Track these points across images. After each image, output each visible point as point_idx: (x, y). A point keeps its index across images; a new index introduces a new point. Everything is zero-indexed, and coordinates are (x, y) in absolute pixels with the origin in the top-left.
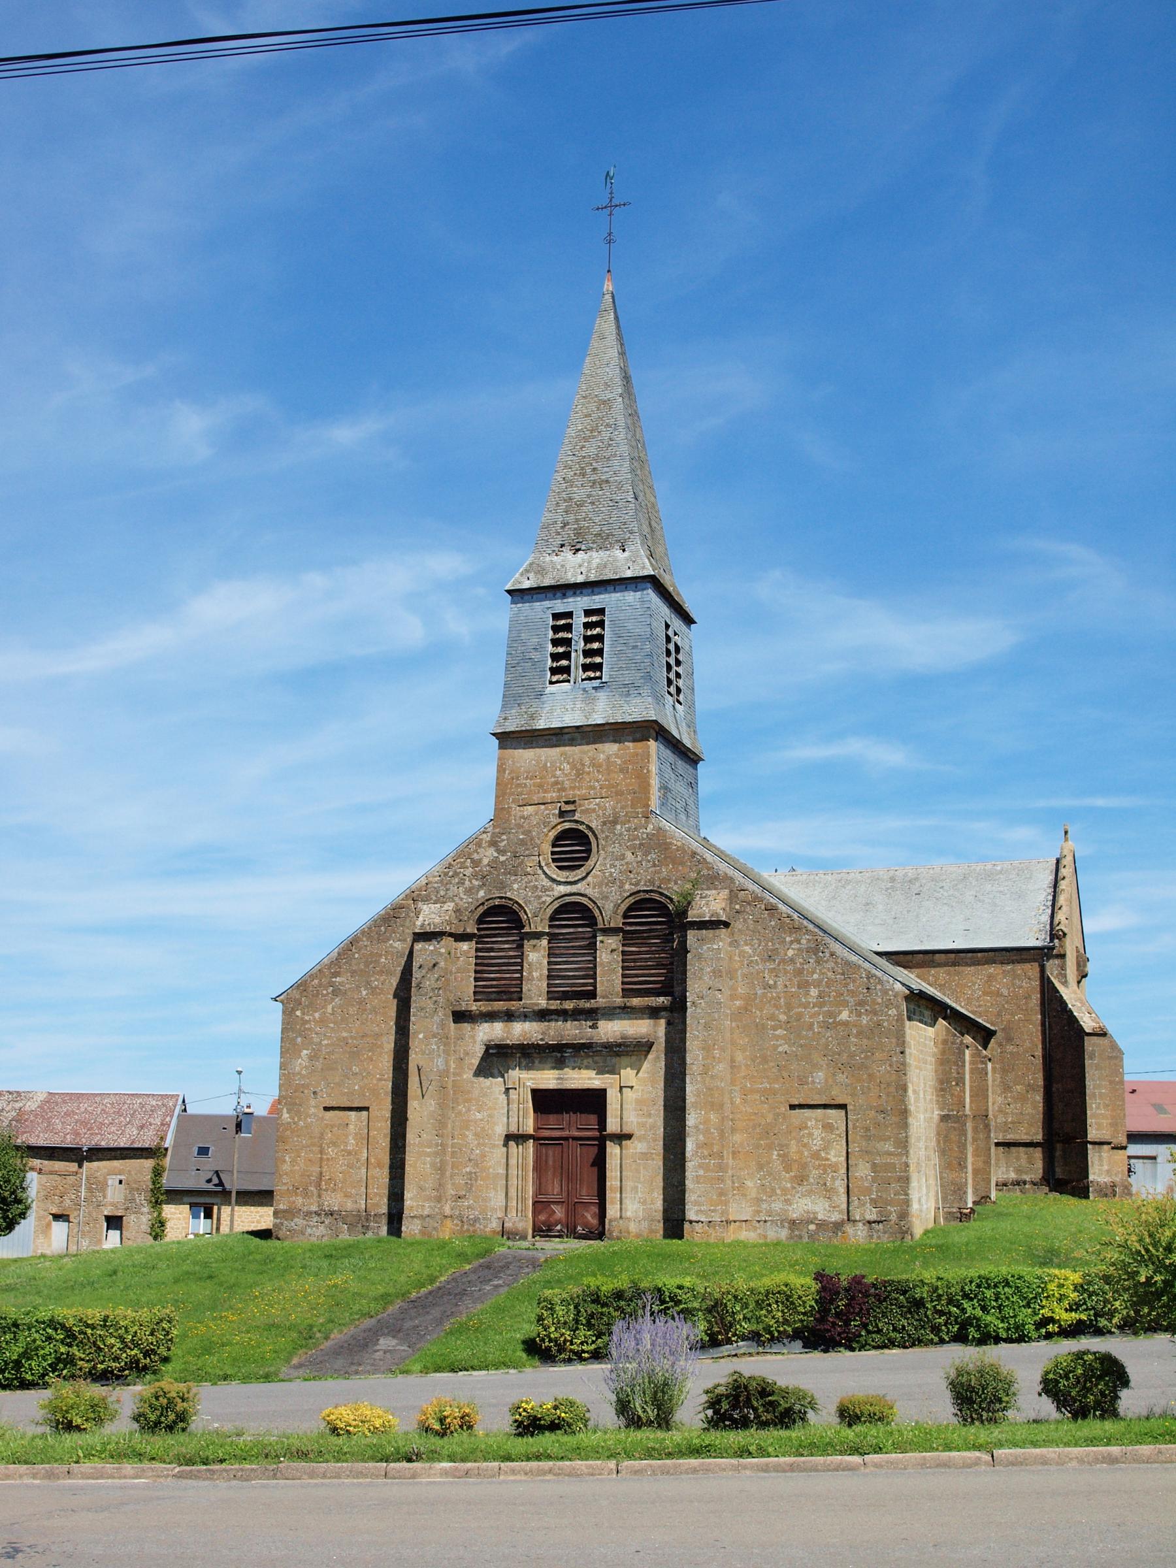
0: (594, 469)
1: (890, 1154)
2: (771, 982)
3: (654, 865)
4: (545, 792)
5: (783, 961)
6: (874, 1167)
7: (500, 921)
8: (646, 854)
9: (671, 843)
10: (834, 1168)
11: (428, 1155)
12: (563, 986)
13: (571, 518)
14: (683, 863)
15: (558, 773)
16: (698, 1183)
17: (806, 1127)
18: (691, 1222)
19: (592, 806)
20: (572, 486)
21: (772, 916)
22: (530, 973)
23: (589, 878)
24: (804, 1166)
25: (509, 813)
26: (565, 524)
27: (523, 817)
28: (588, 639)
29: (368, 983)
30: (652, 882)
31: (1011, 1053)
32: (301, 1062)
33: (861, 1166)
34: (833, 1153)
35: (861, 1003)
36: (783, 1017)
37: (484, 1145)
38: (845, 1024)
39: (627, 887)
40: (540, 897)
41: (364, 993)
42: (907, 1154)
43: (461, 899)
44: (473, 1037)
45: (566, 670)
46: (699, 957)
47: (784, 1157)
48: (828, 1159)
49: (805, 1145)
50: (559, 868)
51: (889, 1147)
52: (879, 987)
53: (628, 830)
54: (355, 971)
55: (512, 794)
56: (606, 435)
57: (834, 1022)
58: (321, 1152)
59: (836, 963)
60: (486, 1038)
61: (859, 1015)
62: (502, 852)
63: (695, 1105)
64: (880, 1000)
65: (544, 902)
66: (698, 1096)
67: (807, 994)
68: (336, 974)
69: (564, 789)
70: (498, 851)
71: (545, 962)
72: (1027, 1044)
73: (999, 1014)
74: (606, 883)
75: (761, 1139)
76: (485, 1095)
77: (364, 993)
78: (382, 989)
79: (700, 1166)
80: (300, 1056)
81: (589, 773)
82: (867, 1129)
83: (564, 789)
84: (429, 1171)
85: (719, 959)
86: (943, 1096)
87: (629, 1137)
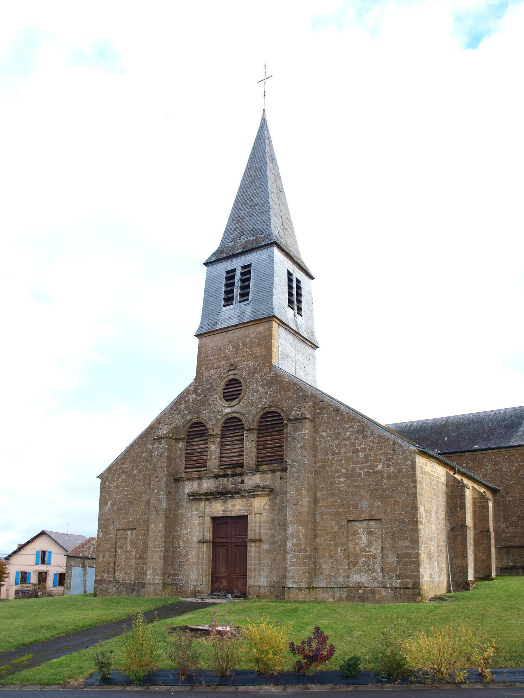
0: (252, 200)
1: (407, 547)
2: (337, 451)
3: (274, 393)
4: (220, 362)
5: (344, 439)
6: (398, 556)
7: (197, 431)
8: (270, 388)
9: (283, 380)
10: (374, 556)
11: (157, 552)
12: (227, 461)
13: (239, 225)
14: (289, 391)
16: (293, 566)
17: (358, 533)
18: (289, 588)
19: (243, 366)
20: (240, 211)
21: (337, 414)
22: (211, 456)
23: (241, 404)
24: (356, 556)
25: (203, 375)
26: (235, 229)
27: (209, 376)
29: (137, 466)
30: (273, 402)
31: (509, 501)
32: (108, 508)
33: (390, 555)
34: (373, 548)
36: (344, 471)
37: (188, 547)
38: (380, 472)
39: (260, 406)
40: (216, 416)
41: (135, 472)
42: (418, 547)
43: (179, 421)
44: (183, 491)
45: (232, 299)
46: (294, 439)
47: (344, 550)
48: (370, 552)
49: (357, 544)
51: (407, 543)
52: (400, 449)
53: (261, 376)
55: (205, 365)
56: (258, 183)
57: (374, 471)
58: (116, 552)
59: (374, 437)
60: (189, 491)
61: (388, 466)
63: (292, 522)
64: (401, 457)
65: (218, 419)
66: (294, 517)
67: (358, 456)
68: (123, 463)
69: (229, 359)
70: (197, 395)
71: (218, 450)
72: (518, 495)
73: (501, 481)
74: (250, 406)
75: (331, 541)
76: (188, 521)
77: (135, 472)
78: (143, 469)
79: (294, 556)
80: (107, 505)
81: (241, 349)
82: (394, 533)
83: (229, 359)
84: (158, 560)
85: (304, 439)
86: (452, 517)
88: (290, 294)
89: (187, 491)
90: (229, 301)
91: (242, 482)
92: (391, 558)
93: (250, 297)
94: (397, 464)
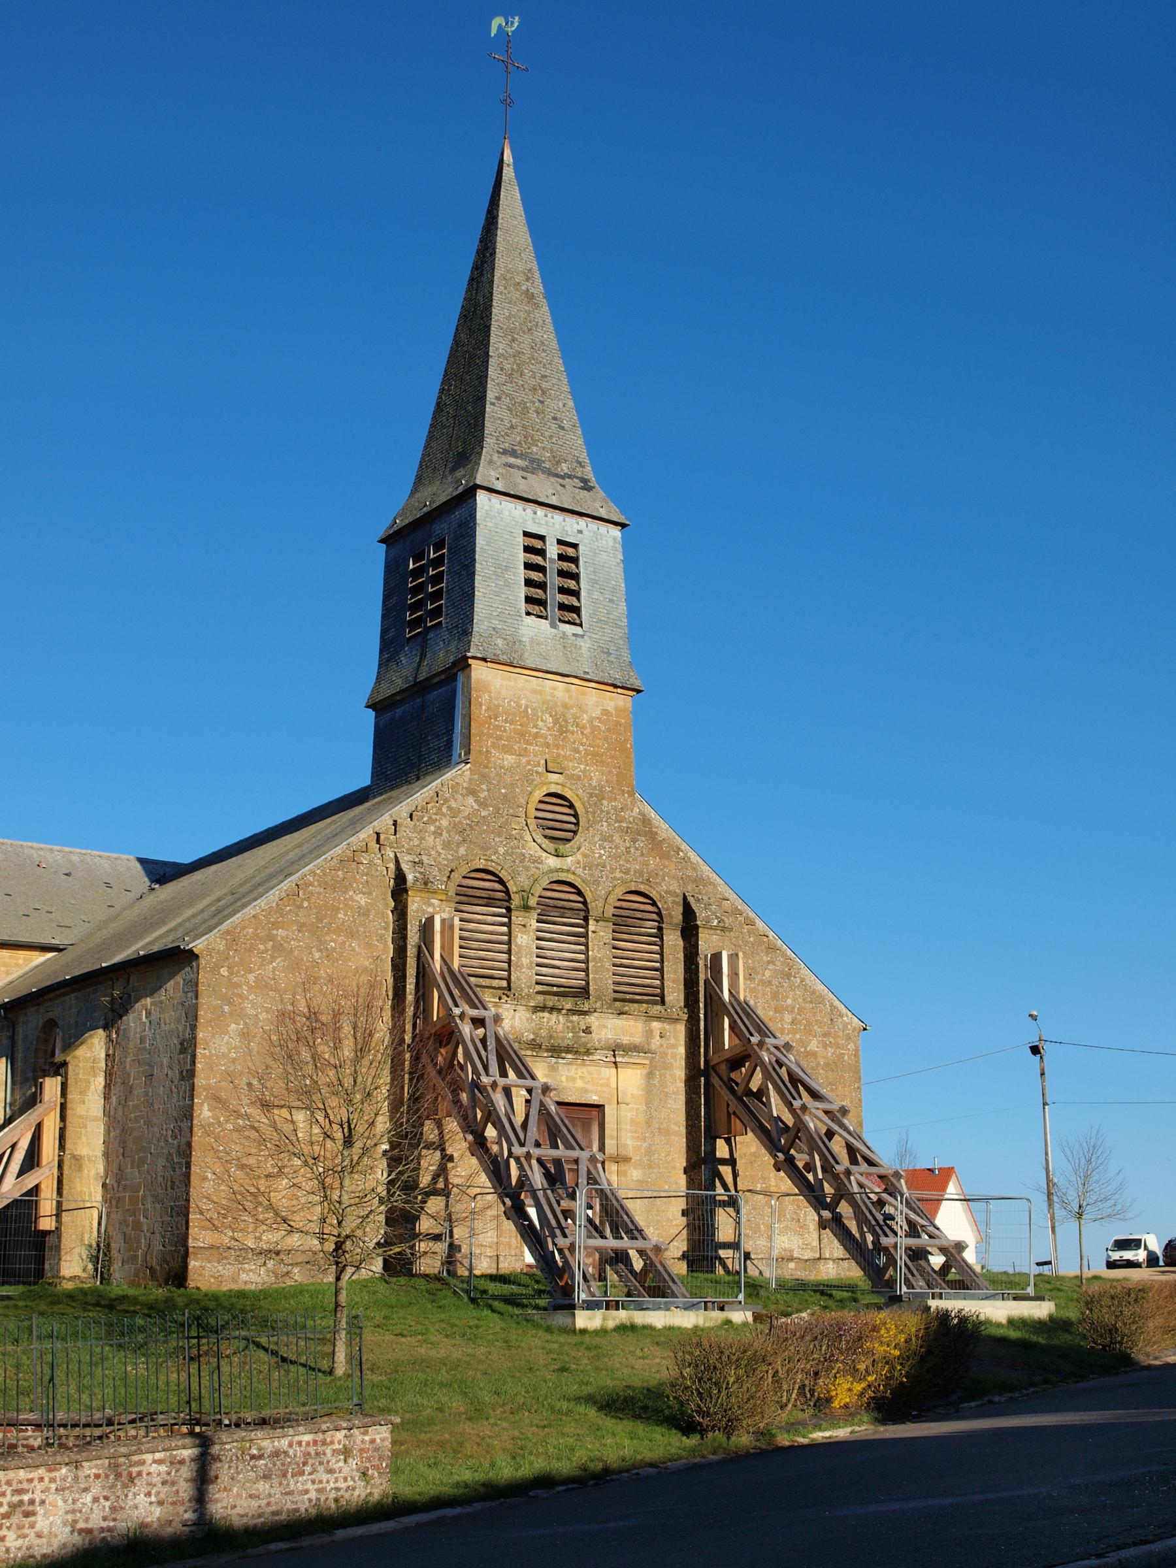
15: (540, 724)
22: (519, 958)
28: (562, 573)
35: (825, 1035)
38: (815, 1054)
43: (440, 854)
50: (545, 837)
54: (303, 925)
57: (806, 1051)
61: (825, 1046)
62: (483, 804)
68: (276, 925)
81: (573, 733)
87: (627, 1160)
94: (838, 1046)
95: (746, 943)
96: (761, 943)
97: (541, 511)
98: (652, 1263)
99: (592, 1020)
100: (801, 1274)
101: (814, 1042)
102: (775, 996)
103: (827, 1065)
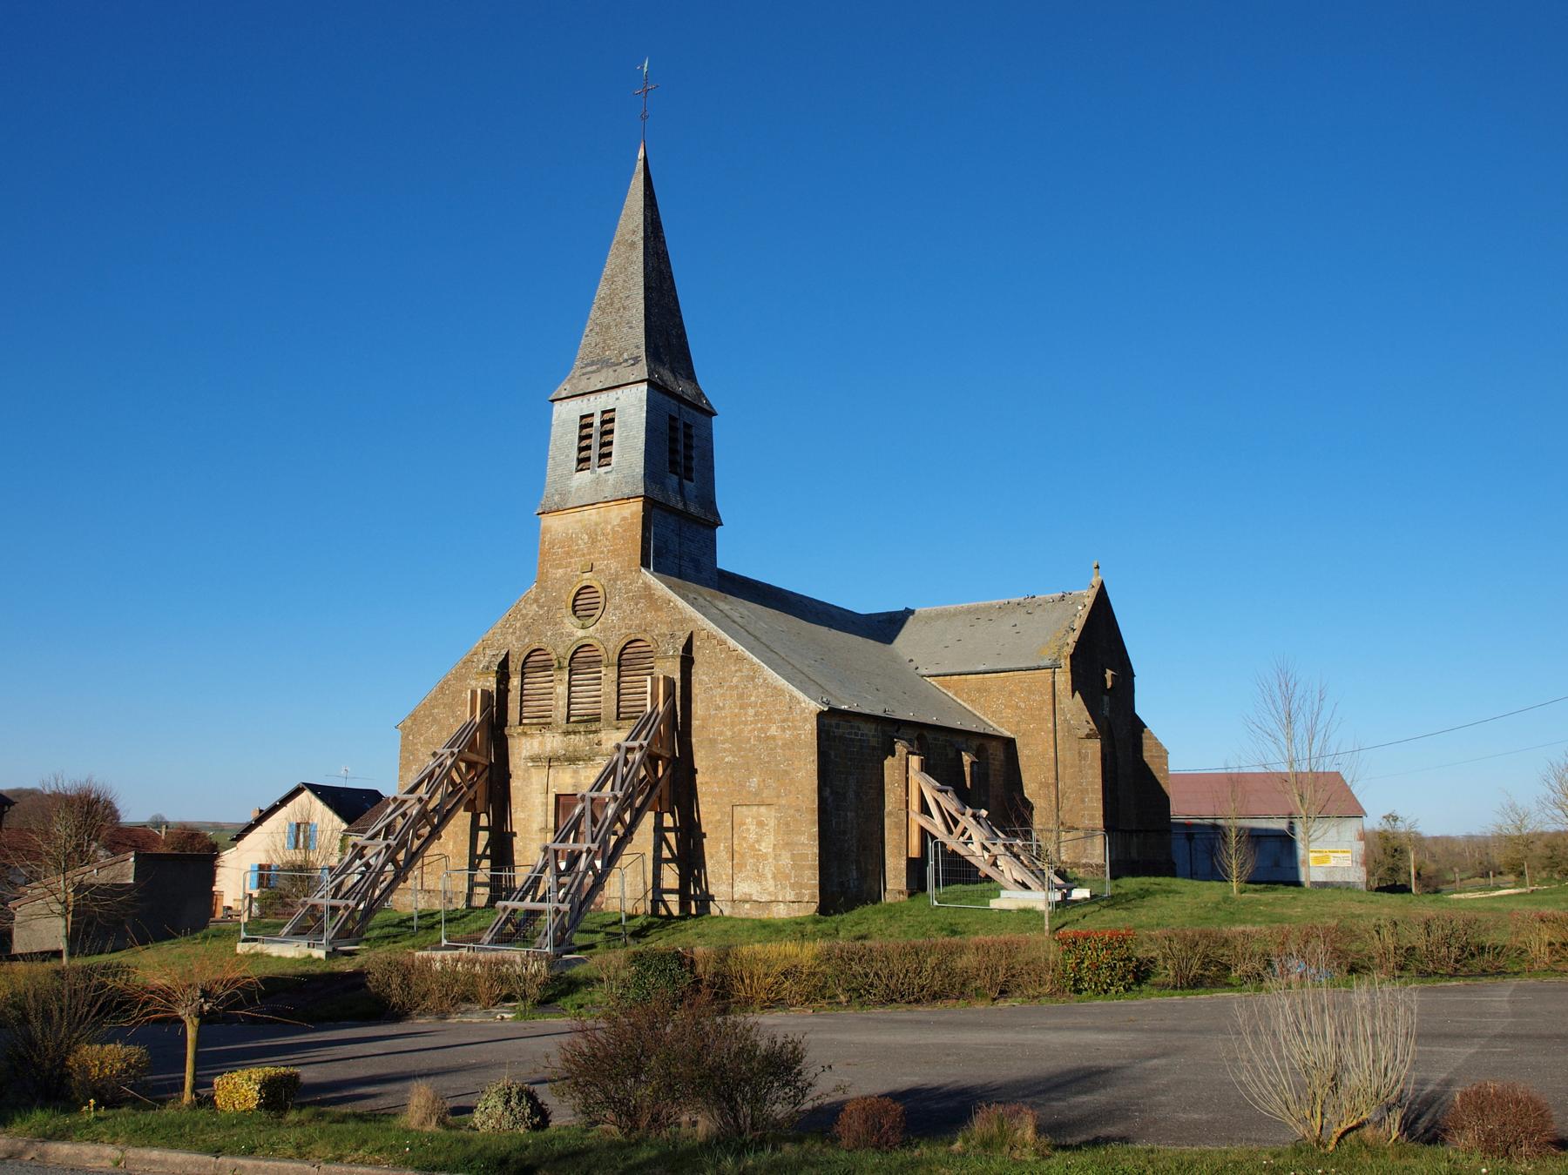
10: (765, 857)
38: (774, 738)
61: (784, 729)
88: (673, 451)
89: (525, 753)
90: (583, 462)
91: (599, 743)
92: (786, 860)
93: (614, 459)
94: (795, 728)
95: (718, 660)
96: (730, 657)
97: (592, 397)
98: (976, 883)
99: (602, 735)
100: (756, 914)
101: (774, 727)
102: (740, 696)
103: (784, 745)
